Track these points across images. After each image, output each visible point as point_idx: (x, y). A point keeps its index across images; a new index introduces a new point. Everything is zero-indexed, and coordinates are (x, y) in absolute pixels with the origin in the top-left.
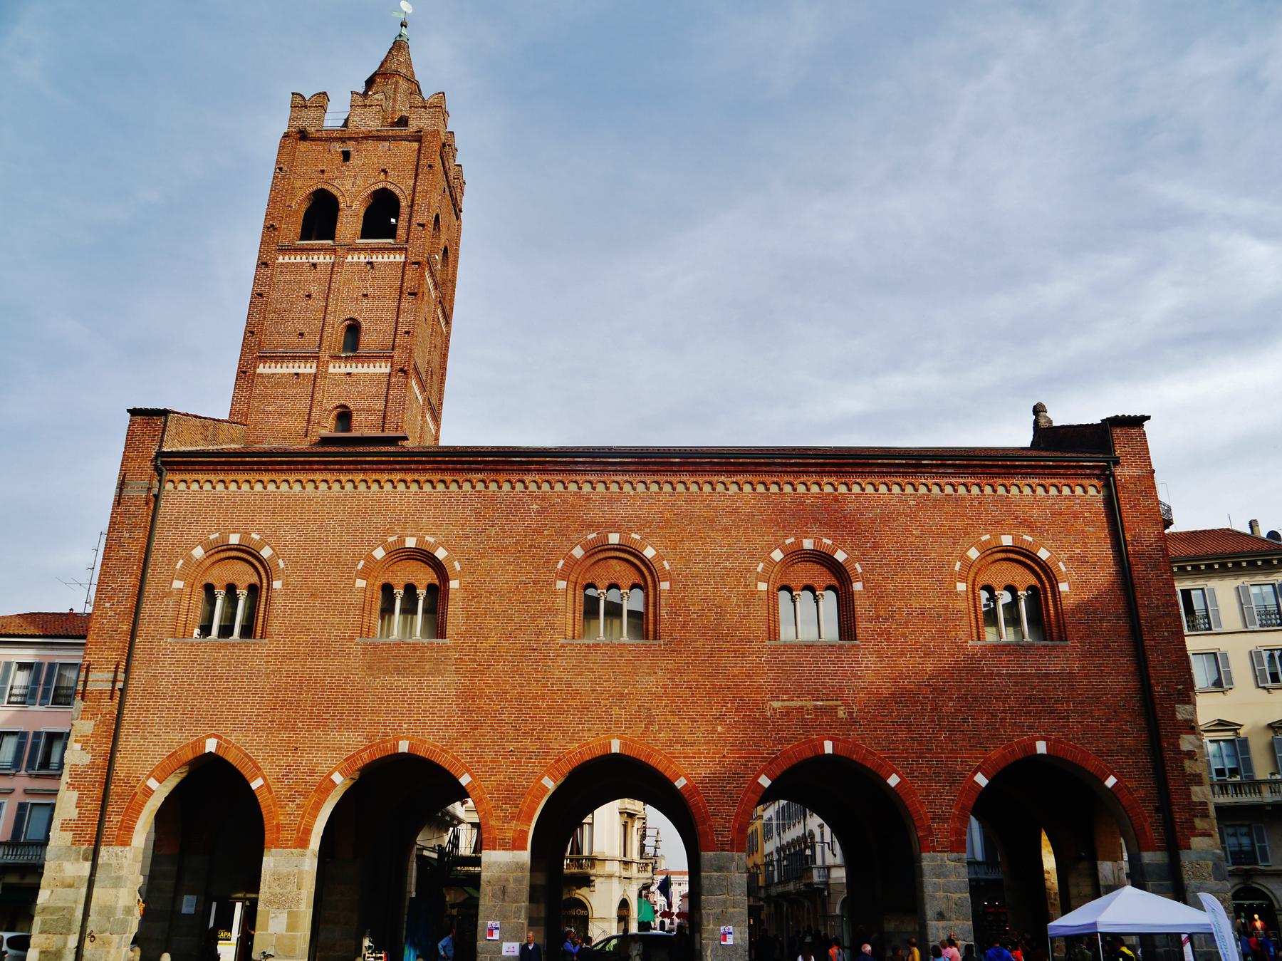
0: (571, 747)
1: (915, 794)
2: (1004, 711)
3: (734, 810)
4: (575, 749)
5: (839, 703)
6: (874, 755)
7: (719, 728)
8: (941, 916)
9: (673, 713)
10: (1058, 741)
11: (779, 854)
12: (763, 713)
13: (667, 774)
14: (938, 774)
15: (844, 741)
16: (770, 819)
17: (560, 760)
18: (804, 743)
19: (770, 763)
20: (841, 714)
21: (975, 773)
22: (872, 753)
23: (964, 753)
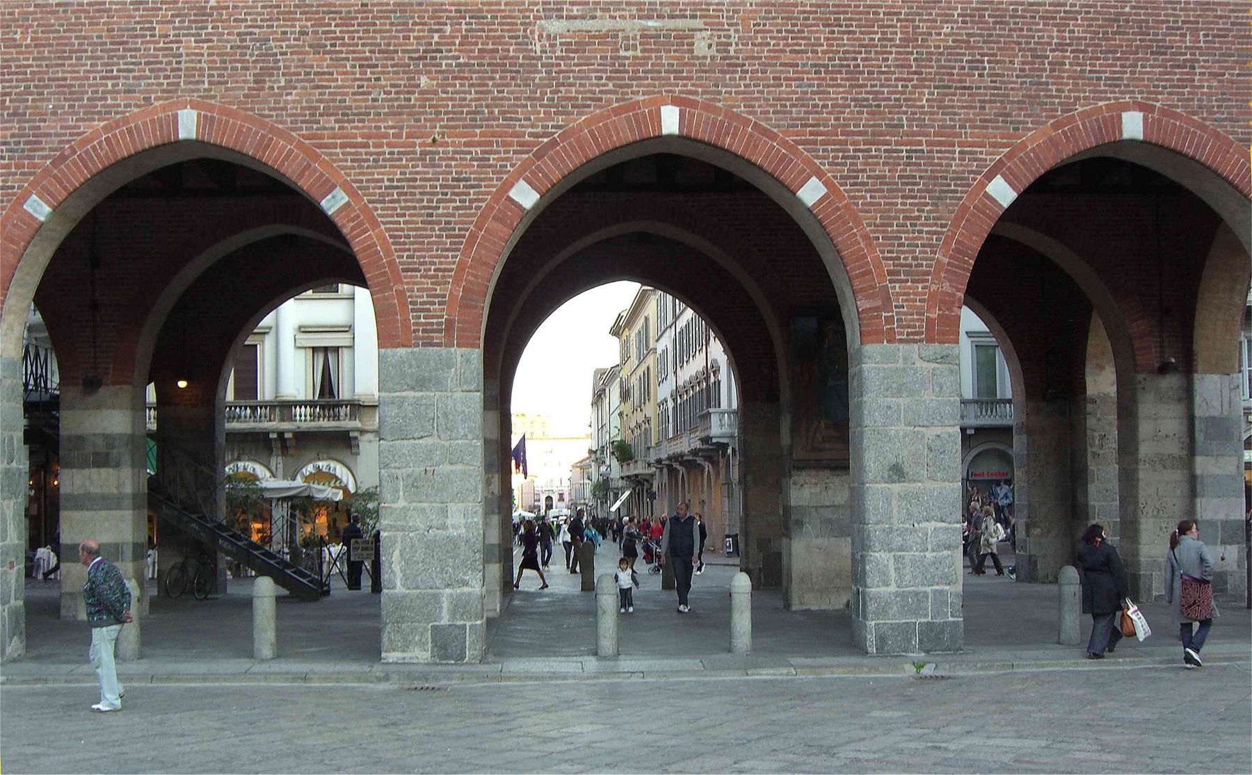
0: (86, 128)
1: (858, 223)
2: (1061, 47)
3: (452, 260)
4: (96, 134)
5: (698, 23)
6: (773, 137)
7: (424, 81)
8: (897, 472)
9: (317, 48)
10: (1167, 112)
11: (675, 400)
12: (523, 44)
13: (305, 184)
14: (909, 180)
15: (708, 107)
16: (665, 351)
17: (63, 158)
18: (617, 111)
19: (538, 156)
20: (701, 47)
21: (990, 177)
22: (766, 132)
23: (968, 134)
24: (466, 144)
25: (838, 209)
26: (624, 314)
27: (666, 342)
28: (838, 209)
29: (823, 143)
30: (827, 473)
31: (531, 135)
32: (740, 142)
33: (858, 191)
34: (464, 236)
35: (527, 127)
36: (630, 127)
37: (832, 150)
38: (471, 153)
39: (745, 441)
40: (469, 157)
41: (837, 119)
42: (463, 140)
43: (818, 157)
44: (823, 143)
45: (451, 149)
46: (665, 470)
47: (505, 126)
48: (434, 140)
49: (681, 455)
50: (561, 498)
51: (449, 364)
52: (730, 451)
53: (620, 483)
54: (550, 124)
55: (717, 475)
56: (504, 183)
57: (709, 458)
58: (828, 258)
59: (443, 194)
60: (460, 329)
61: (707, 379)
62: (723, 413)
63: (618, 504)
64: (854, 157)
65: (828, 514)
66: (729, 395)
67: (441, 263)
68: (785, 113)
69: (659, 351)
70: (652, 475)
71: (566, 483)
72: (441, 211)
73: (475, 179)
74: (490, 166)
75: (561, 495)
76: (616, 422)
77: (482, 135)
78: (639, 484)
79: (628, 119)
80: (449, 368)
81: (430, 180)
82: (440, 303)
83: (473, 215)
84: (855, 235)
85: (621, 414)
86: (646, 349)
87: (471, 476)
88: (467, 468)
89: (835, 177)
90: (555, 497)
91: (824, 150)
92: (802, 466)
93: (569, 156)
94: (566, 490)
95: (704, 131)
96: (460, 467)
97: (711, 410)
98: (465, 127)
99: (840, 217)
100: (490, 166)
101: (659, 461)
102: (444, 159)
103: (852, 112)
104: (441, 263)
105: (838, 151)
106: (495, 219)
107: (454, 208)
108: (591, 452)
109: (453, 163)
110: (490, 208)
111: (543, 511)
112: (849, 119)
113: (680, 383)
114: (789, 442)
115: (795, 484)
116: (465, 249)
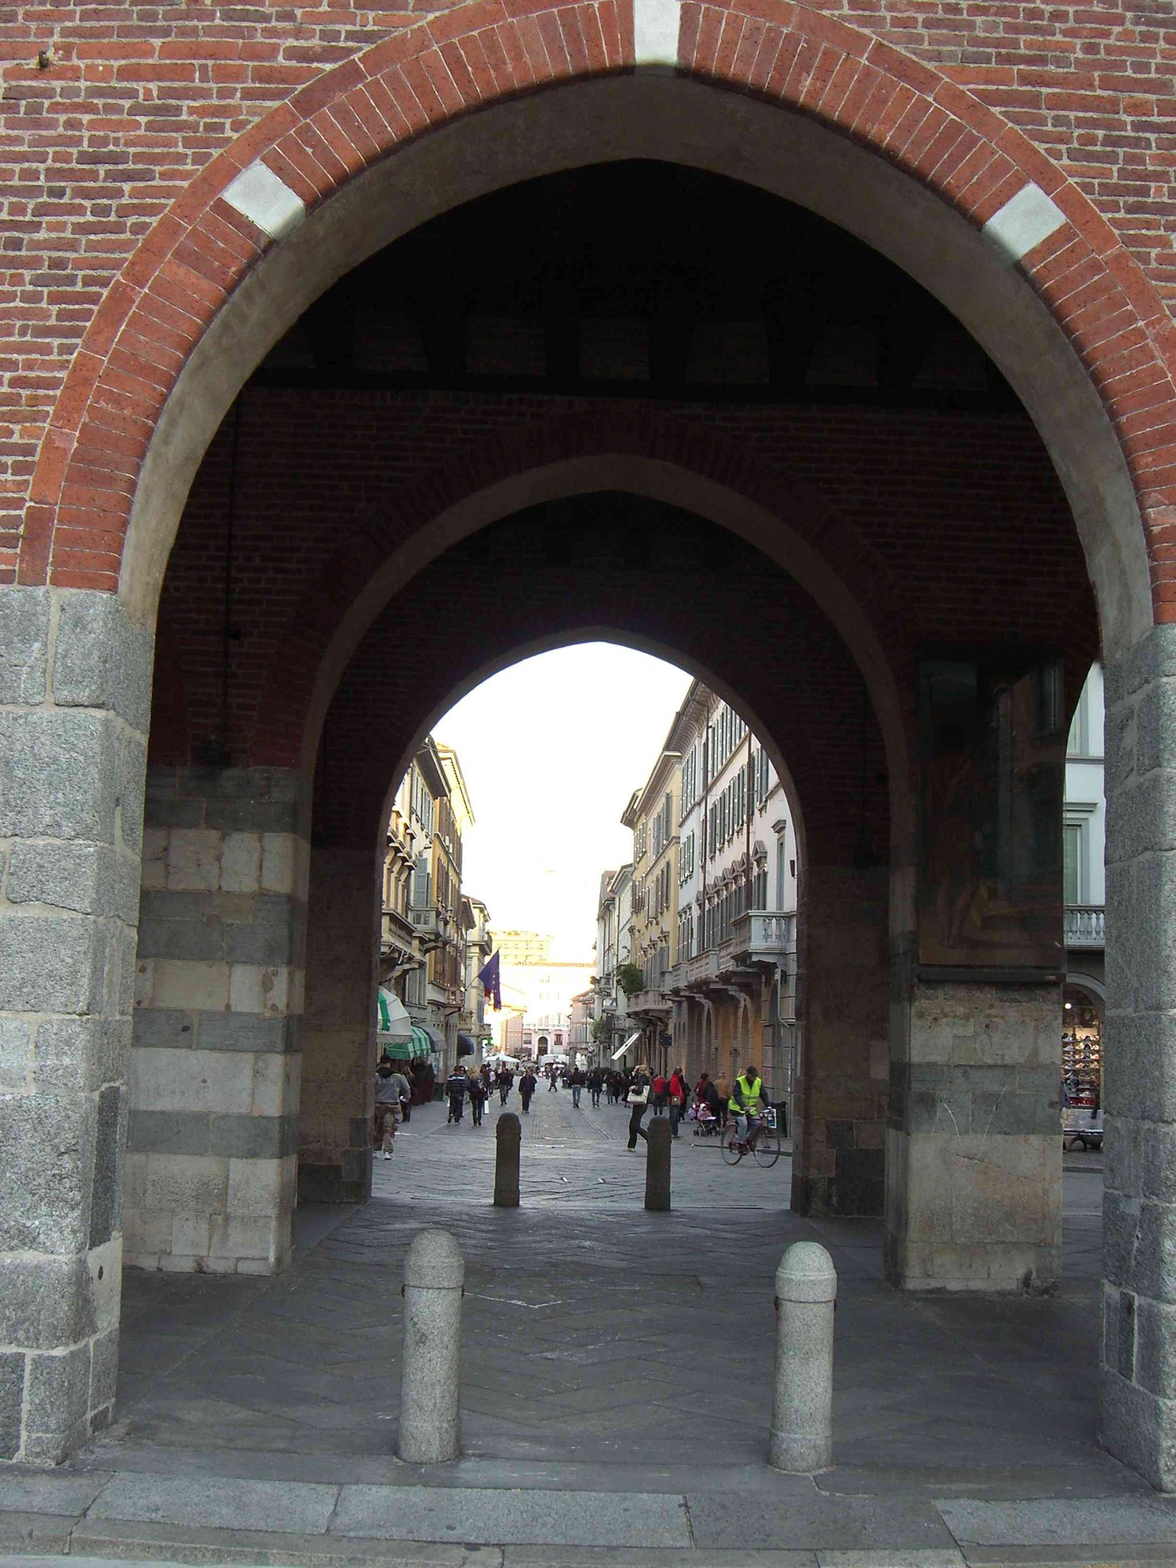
1: (1148, 303)
3: (59, 358)
6: (927, 81)
19: (307, 104)
22: (903, 69)
24: (125, 74)
25: (1096, 267)
26: (640, 794)
27: (694, 825)
28: (1096, 267)
29: (1055, 103)
30: (989, 995)
31: (291, 53)
32: (840, 88)
33: (1149, 225)
34: (94, 299)
35: (284, 34)
36: (552, 40)
37: (1080, 123)
38: (131, 94)
39: (810, 936)
40: (127, 103)
41: (1090, 49)
42: (116, 64)
43: (1043, 138)
44: (1055, 103)
45: (83, 84)
46: (685, 1005)
47: (223, 32)
48: (44, 64)
49: (706, 982)
50: (558, 1041)
51: (26, 628)
52: (778, 976)
53: (628, 1023)
54: (344, 28)
55: (758, 1011)
56: (213, 171)
57: (746, 987)
58: (1054, 417)
59: (52, 192)
60: (66, 539)
61: (747, 871)
62: (770, 917)
63: (623, 1049)
64: (1136, 143)
65: (990, 1083)
66: (784, 892)
67: (29, 365)
68: (955, 26)
69: (683, 840)
70: (668, 1012)
71: (565, 1022)
72: (42, 235)
73: (138, 158)
74: (180, 127)
75: (559, 1036)
76: (626, 939)
77: (166, 51)
78: (649, 1022)
79: (546, 24)
80: (27, 640)
81: (23, 157)
82: (19, 469)
83: (124, 246)
84: (1141, 334)
85: (631, 930)
86: (666, 838)
87: (61, 939)
88: (51, 914)
89: (1088, 188)
90: (551, 1040)
91: (1058, 121)
92: (936, 978)
93: (388, 108)
94: (565, 1031)
95: (745, 59)
96: (33, 912)
97: (752, 912)
98: (125, 32)
99: (1097, 289)
100: (180, 127)
101: (676, 992)
102: (65, 109)
103: (1127, 35)
104: (29, 365)
105: (1094, 123)
106: (181, 255)
107: (81, 228)
108: (595, 981)
109: (86, 118)
110: (170, 228)
111: (534, 1057)
112: (1122, 51)
113: (710, 881)
114: (910, 925)
115: (921, 1015)
116: (96, 331)
